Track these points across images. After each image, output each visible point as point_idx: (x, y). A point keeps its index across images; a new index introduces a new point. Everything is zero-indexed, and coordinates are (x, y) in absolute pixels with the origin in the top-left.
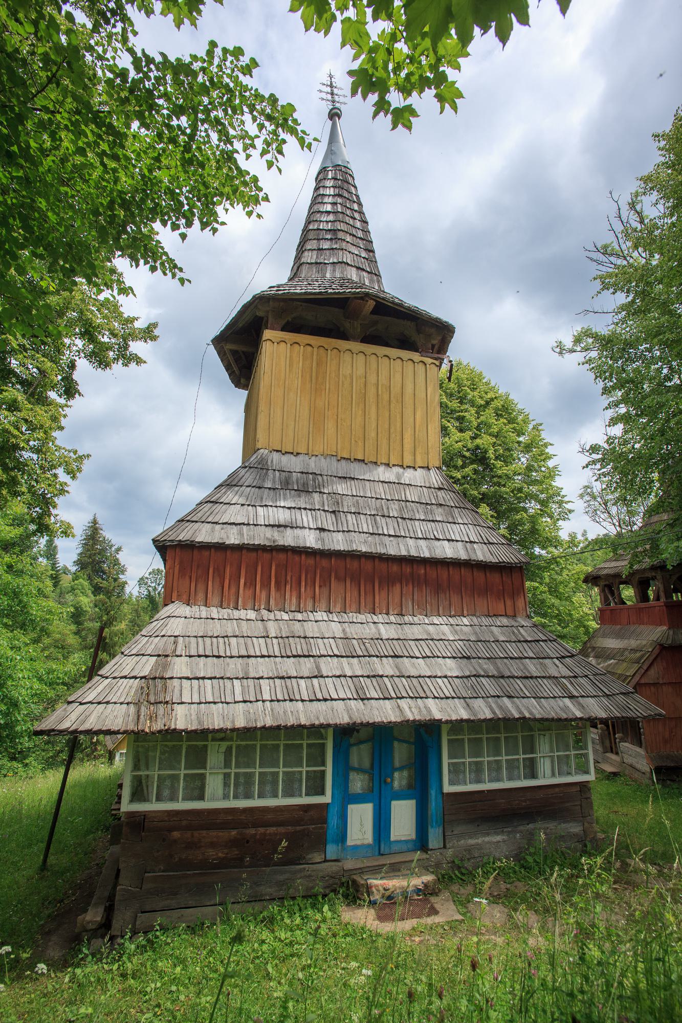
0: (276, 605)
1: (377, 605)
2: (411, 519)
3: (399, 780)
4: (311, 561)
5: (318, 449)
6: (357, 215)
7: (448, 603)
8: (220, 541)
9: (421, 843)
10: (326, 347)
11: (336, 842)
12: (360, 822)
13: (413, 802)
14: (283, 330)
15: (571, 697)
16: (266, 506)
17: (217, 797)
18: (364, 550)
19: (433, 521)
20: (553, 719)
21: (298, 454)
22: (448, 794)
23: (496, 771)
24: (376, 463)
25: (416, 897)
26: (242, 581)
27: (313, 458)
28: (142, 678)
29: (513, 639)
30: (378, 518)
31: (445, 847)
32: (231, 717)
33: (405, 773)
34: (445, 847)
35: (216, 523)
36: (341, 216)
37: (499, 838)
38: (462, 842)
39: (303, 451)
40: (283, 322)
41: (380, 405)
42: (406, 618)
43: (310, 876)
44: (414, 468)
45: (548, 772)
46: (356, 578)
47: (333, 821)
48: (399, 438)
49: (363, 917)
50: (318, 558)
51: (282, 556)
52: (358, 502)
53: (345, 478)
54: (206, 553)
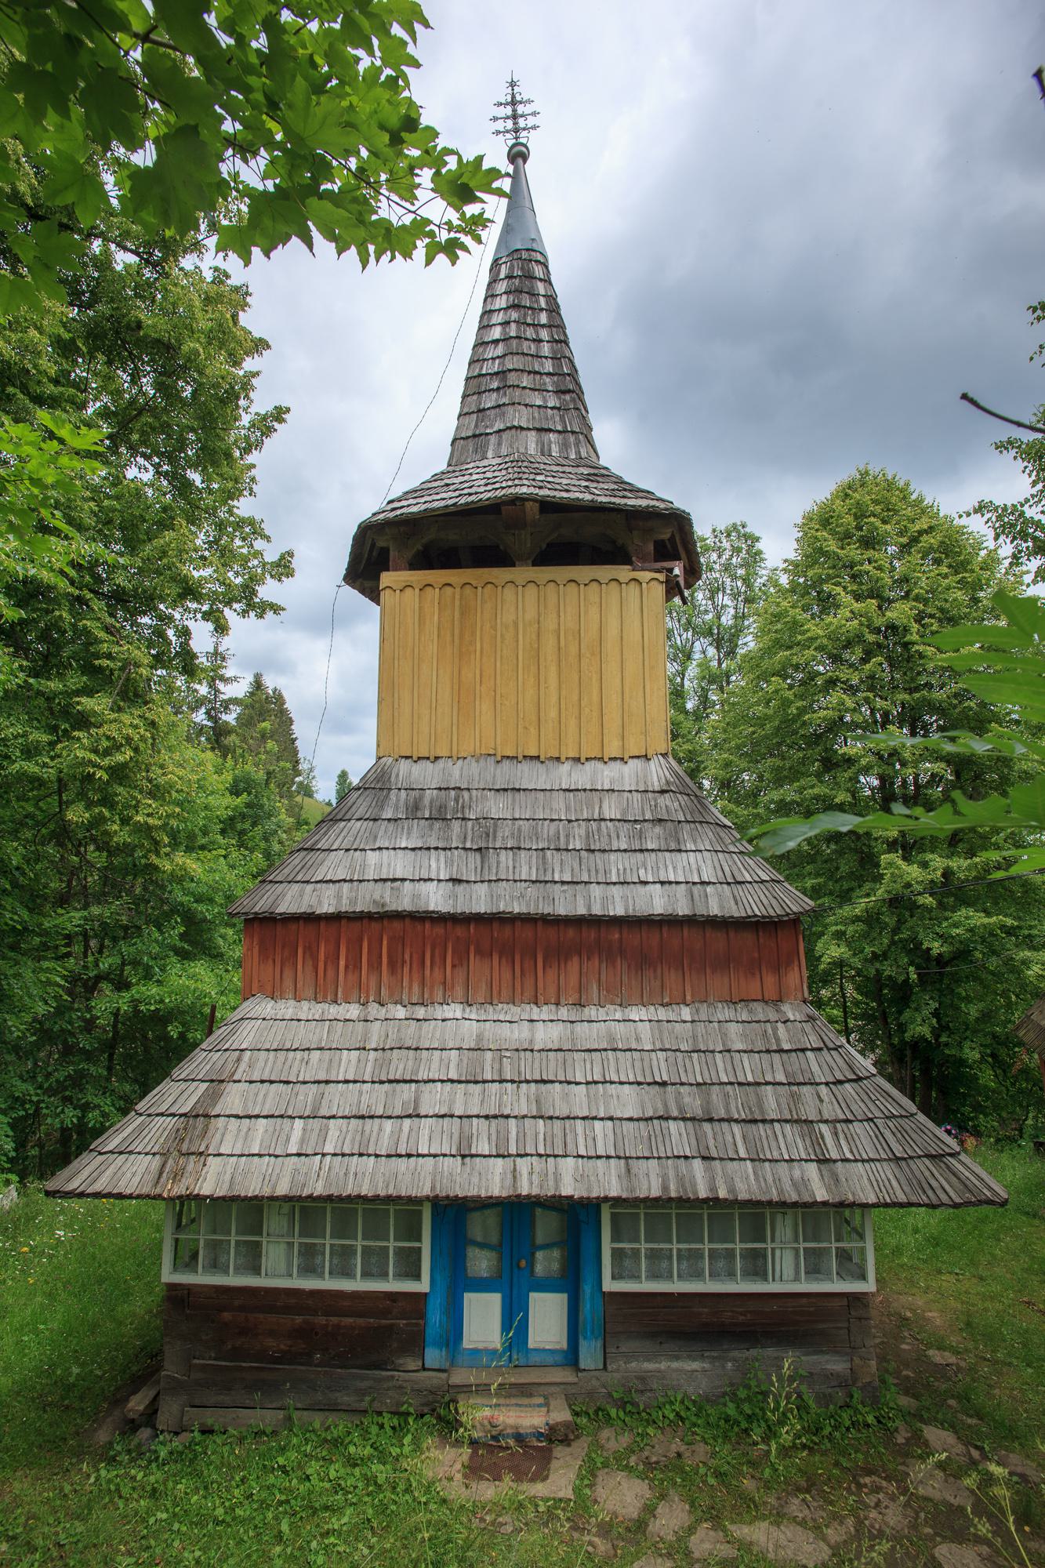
0: (391, 995)
1: (540, 991)
2: (604, 851)
3: (546, 1262)
4: (439, 930)
5: (466, 749)
6: (544, 334)
7: (658, 983)
8: (309, 911)
9: (571, 1357)
10: (474, 583)
11: (438, 1345)
12: (482, 1319)
13: (565, 1296)
14: (413, 566)
15: (823, 1161)
16: (380, 849)
17: (279, 1271)
18: (517, 910)
19: (641, 851)
20: (770, 1203)
21: (437, 758)
22: (612, 1294)
23: (692, 1265)
24: (558, 759)
25: (536, 1444)
26: (342, 963)
27: (460, 762)
28: (181, 1115)
29: (759, 1046)
30: (549, 853)
31: (605, 1367)
32: (274, 1178)
33: (556, 1253)
34: (605, 1367)
35: (308, 882)
36: (514, 342)
37: (696, 1365)
38: (634, 1364)
39: (444, 753)
40: (409, 554)
41: (563, 663)
42: (586, 1010)
43: (401, 1387)
44: (622, 759)
45: (788, 1271)
46: (507, 952)
47: (435, 1317)
48: (596, 714)
49: (441, 1463)
50: (449, 924)
51: (397, 925)
52: (519, 830)
53: (505, 790)
54: (293, 927)
